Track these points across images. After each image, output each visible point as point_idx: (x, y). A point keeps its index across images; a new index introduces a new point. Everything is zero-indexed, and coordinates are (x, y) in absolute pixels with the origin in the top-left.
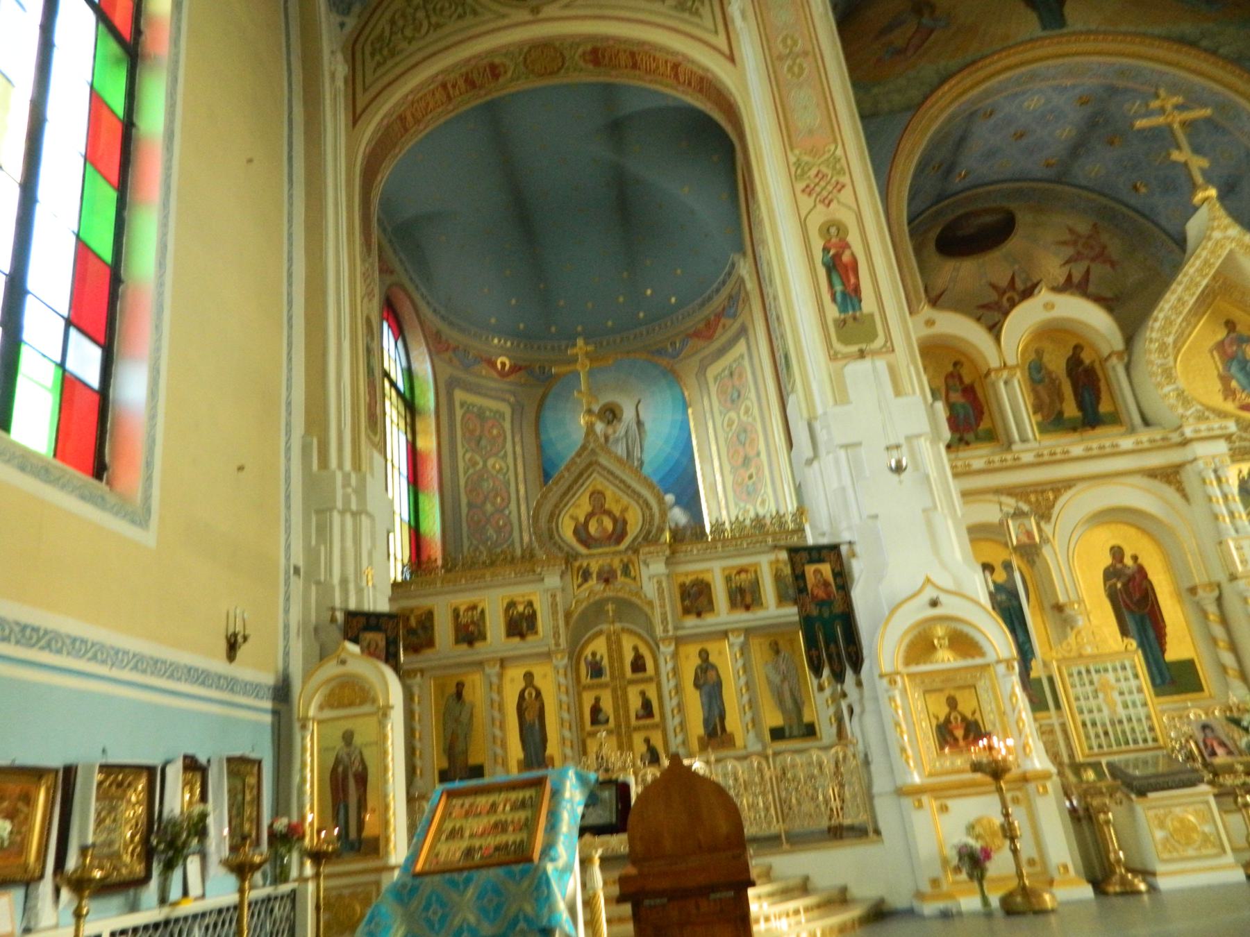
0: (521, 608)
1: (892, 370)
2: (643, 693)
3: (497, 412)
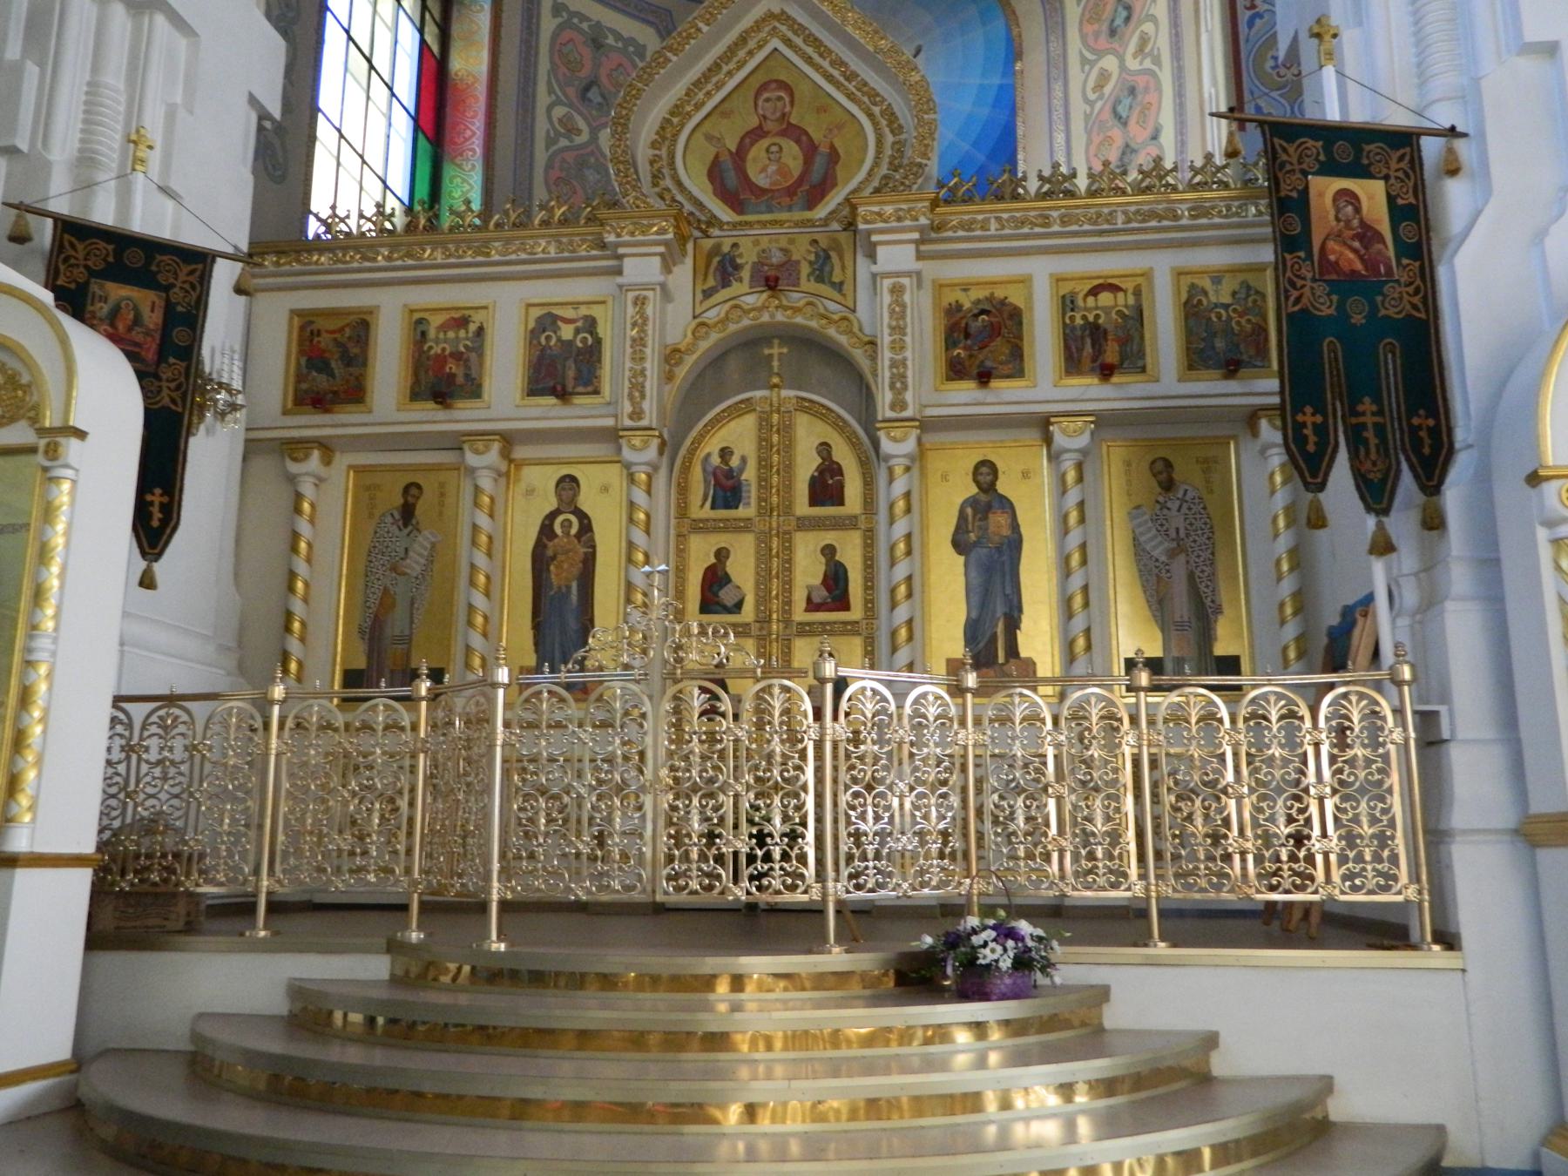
0: (567, 332)
2: (829, 551)
3: (631, 41)
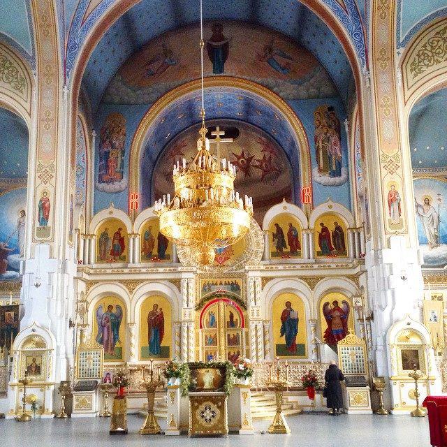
1: (51, 250)
